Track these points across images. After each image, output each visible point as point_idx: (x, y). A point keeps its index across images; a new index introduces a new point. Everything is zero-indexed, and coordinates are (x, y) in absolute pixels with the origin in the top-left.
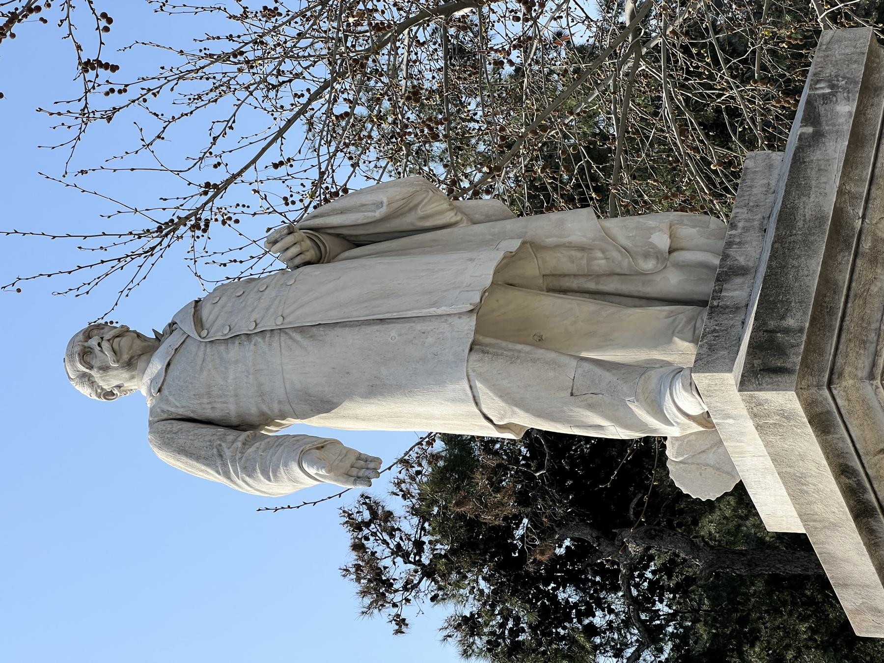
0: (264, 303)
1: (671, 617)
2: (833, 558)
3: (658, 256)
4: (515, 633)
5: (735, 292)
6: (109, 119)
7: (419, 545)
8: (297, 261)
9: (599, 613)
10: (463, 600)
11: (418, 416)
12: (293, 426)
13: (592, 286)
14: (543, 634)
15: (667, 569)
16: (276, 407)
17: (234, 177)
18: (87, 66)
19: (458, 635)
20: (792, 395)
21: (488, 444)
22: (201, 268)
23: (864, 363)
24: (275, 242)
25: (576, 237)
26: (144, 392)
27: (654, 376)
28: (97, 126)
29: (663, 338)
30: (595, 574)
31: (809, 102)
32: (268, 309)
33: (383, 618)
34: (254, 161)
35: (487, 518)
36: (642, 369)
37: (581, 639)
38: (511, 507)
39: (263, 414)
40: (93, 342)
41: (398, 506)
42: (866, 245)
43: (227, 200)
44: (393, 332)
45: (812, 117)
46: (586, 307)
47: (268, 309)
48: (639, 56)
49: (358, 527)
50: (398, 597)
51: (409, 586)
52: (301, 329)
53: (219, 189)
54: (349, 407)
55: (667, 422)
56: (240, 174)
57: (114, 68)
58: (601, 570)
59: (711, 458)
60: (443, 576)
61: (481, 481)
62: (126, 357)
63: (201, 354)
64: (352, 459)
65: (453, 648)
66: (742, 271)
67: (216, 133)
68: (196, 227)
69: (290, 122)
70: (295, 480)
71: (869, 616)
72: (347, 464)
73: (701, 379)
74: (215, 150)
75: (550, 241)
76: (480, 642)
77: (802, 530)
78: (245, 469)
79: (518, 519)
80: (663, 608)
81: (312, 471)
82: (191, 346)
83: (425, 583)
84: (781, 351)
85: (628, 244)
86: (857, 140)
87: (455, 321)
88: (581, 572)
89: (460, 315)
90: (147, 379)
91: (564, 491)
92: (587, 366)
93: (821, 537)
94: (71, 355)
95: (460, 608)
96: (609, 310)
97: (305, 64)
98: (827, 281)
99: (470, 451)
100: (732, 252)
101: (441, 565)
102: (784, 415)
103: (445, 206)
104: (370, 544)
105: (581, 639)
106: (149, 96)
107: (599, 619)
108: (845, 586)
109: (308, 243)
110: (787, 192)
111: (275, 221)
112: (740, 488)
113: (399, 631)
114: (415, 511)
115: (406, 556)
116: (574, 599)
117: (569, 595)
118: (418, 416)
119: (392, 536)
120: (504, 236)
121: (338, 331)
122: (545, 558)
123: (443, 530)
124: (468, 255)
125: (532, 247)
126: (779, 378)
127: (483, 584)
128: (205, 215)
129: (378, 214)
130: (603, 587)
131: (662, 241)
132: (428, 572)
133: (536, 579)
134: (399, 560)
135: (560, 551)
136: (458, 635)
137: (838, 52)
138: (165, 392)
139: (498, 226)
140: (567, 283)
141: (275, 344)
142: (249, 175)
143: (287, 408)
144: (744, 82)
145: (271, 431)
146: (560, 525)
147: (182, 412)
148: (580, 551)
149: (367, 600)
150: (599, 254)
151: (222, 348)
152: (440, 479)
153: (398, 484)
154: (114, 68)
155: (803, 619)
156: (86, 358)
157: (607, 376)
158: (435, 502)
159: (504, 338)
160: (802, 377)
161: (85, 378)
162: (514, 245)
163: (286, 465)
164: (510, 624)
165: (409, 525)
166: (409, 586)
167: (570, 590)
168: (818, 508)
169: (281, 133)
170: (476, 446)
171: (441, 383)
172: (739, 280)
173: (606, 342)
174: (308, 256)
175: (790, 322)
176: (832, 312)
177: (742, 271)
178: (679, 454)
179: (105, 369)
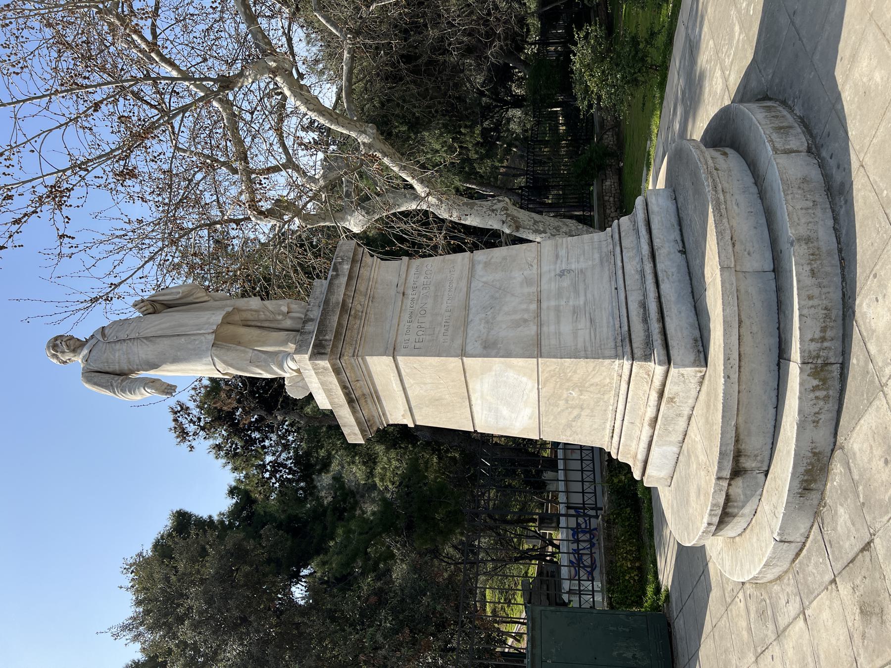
0: (131, 328)
1: (294, 441)
2: (341, 417)
3: (283, 314)
4: (235, 449)
5: (310, 327)
6: (70, 257)
7: (199, 419)
8: (145, 313)
9: (267, 441)
10: (215, 438)
11: (192, 370)
12: (143, 374)
13: (259, 324)
14: (246, 449)
15: (291, 425)
16: (135, 367)
17: (123, 281)
18: (62, 236)
19: (214, 451)
20: (327, 362)
21: (226, 382)
22: (109, 315)
23: (351, 351)
24: (136, 305)
25: (254, 307)
26: (80, 361)
27: (281, 356)
28: (65, 260)
29: (284, 343)
30: (266, 427)
31: (334, 264)
32: (132, 330)
33: (185, 446)
34: (131, 276)
35: (225, 408)
36: (276, 354)
37: (260, 450)
38: (235, 404)
39: (130, 370)
40: (58, 342)
41: (191, 405)
42: (353, 312)
43: (120, 290)
44: (183, 340)
45: (335, 269)
46: (256, 332)
47: (132, 330)
48: (281, 246)
49: (176, 413)
50: (191, 438)
51: (195, 434)
52: (146, 338)
53: (116, 286)
54: (165, 367)
55: (285, 372)
56: (125, 280)
57: (73, 238)
58: (268, 426)
59: (301, 384)
60: (208, 430)
61: (223, 395)
62: (72, 348)
63: (104, 347)
64: (166, 386)
65: (212, 455)
66: (312, 320)
67: (115, 264)
68: (107, 300)
69: (146, 262)
70: (142, 394)
71: (352, 436)
72: (164, 387)
73: (297, 357)
74: (116, 271)
75: (244, 308)
76: (222, 453)
77: (330, 408)
78: (122, 390)
79: (237, 408)
80: (290, 438)
81: (149, 391)
82: (100, 344)
83: (202, 433)
84: (324, 347)
85: (273, 310)
86: (350, 278)
87: (207, 336)
88: (260, 427)
89: (209, 333)
90: (81, 356)
91: (255, 398)
92: (256, 352)
93: (337, 410)
94: (48, 347)
95: (215, 441)
96: (265, 333)
97: (154, 241)
98: (339, 324)
99: (219, 384)
100: (308, 313)
101: (208, 426)
102: (325, 369)
103: (204, 294)
104: (180, 419)
105: (260, 450)
106: (88, 249)
107: (267, 443)
108: (345, 426)
109: (150, 306)
110: (327, 294)
111: (139, 298)
112: (311, 394)
113: (191, 451)
114: (198, 406)
115: (194, 423)
116: (258, 436)
117: (256, 435)
118: (192, 370)
119: (189, 416)
120: (226, 306)
121: (161, 339)
122: (247, 422)
123: (208, 413)
124: (212, 312)
125: (236, 310)
126: (323, 356)
127: (224, 432)
128: (110, 295)
129: (178, 296)
130: (269, 432)
131: (284, 309)
132: (203, 429)
133: (244, 430)
134: (192, 424)
135: (253, 420)
136: (214, 451)
137: (344, 248)
138: (89, 361)
139: (224, 302)
140: (250, 323)
141: (135, 344)
142: (128, 281)
143: (140, 367)
144: (316, 257)
145: (133, 376)
146: (253, 410)
147: (96, 369)
148: (261, 419)
149: (179, 440)
150: (262, 313)
151: (113, 345)
152: (208, 394)
153: (192, 397)
154: (73, 238)
155: (339, 439)
156: (56, 348)
157: (264, 356)
158: (206, 403)
159: (226, 342)
160: (330, 356)
161: (54, 356)
162: (230, 309)
163: (138, 388)
164: (234, 446)
165: (195, 412)
166: (195, 434)
167: (256, 433)
168: (336, 400)
169: (143, 266)
170: (222, 383)
171: (201, 358)
172: (311, 323)
173: (264, 344)
174: (150, 311)
175: (327, 337)
176: (341, 334)
177: (312, 320)
178: (289, 383)
179: (63, 352)
